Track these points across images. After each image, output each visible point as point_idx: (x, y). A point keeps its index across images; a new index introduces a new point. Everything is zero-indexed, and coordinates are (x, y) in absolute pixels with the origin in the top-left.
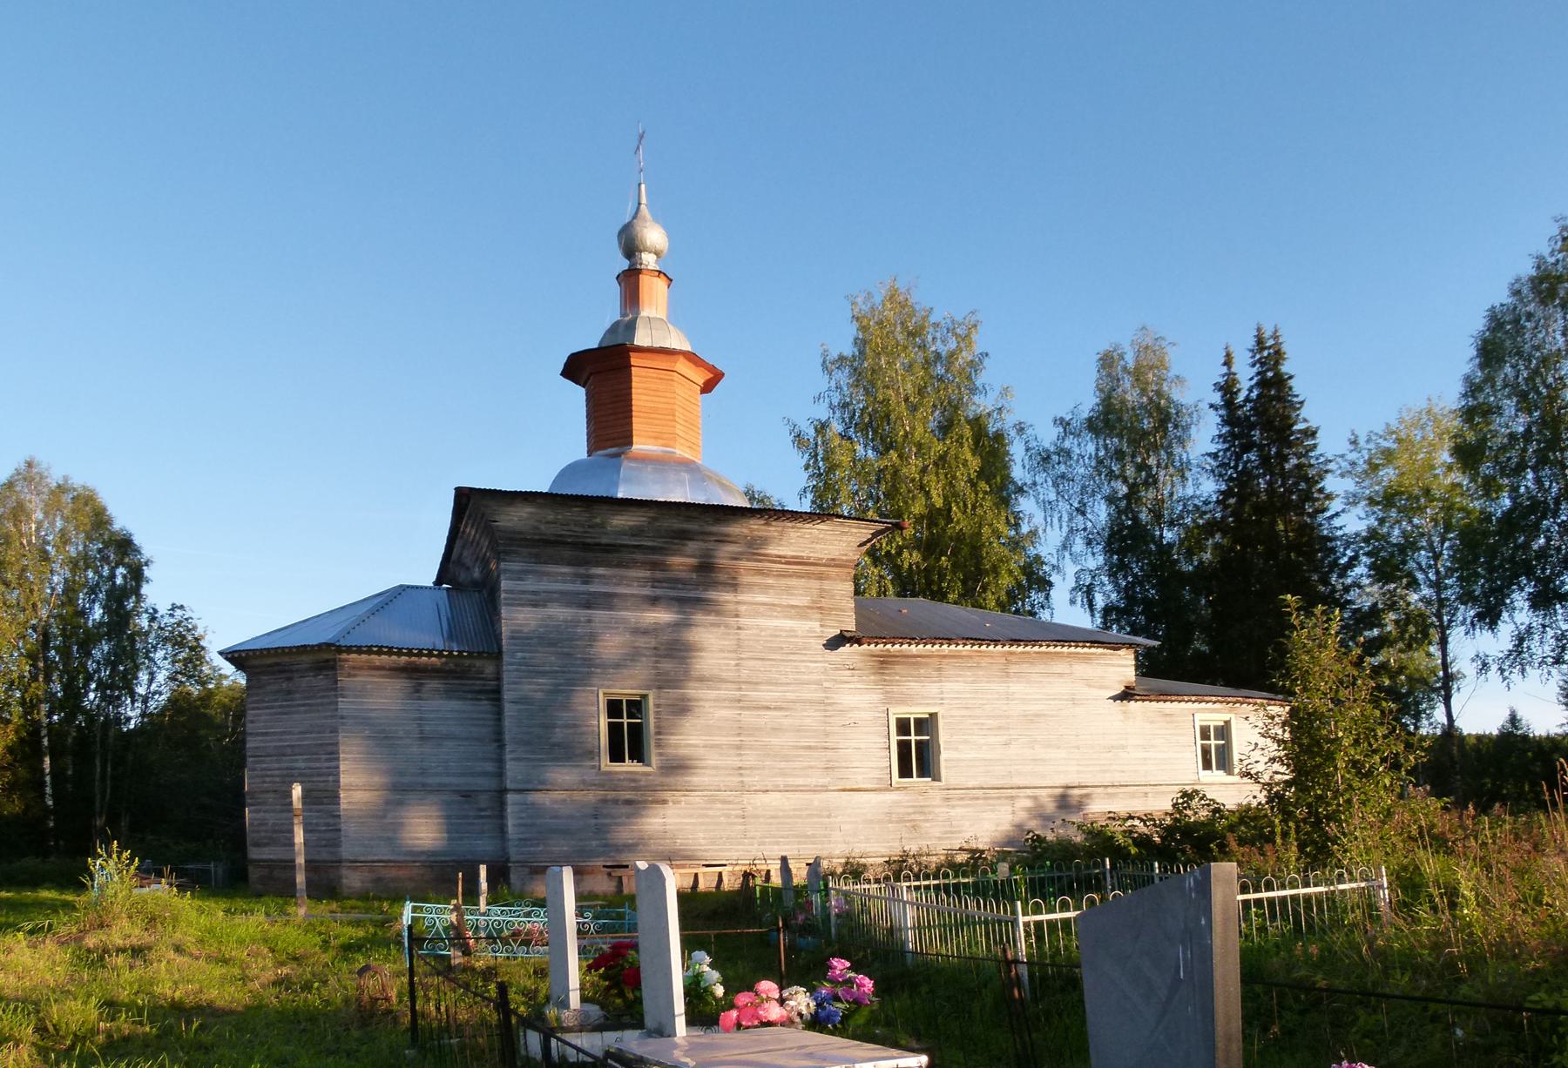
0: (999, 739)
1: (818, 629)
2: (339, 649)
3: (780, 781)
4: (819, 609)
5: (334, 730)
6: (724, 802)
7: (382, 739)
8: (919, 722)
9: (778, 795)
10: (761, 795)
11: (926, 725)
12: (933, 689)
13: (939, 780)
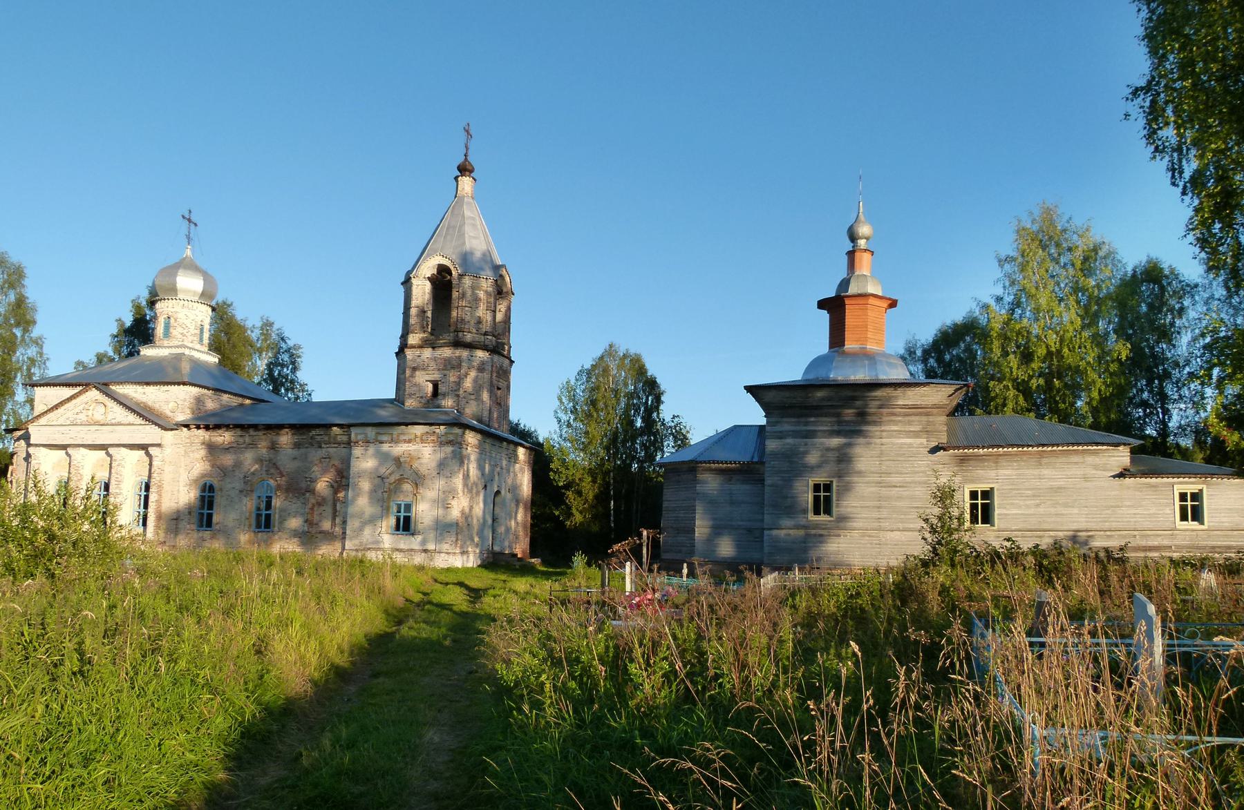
0: (1033, 502)
1: (924, 443)
2: (697, 462)
3: (901, 526)
4: (926, 432)
5: (695, 500)
6: (869, 536)
7: (712, 503)
8: (983, 492)
9: (899, 533)
10: (889, 533)
11: (987, 494)
12: (992, 473)
13: (994, 526)
